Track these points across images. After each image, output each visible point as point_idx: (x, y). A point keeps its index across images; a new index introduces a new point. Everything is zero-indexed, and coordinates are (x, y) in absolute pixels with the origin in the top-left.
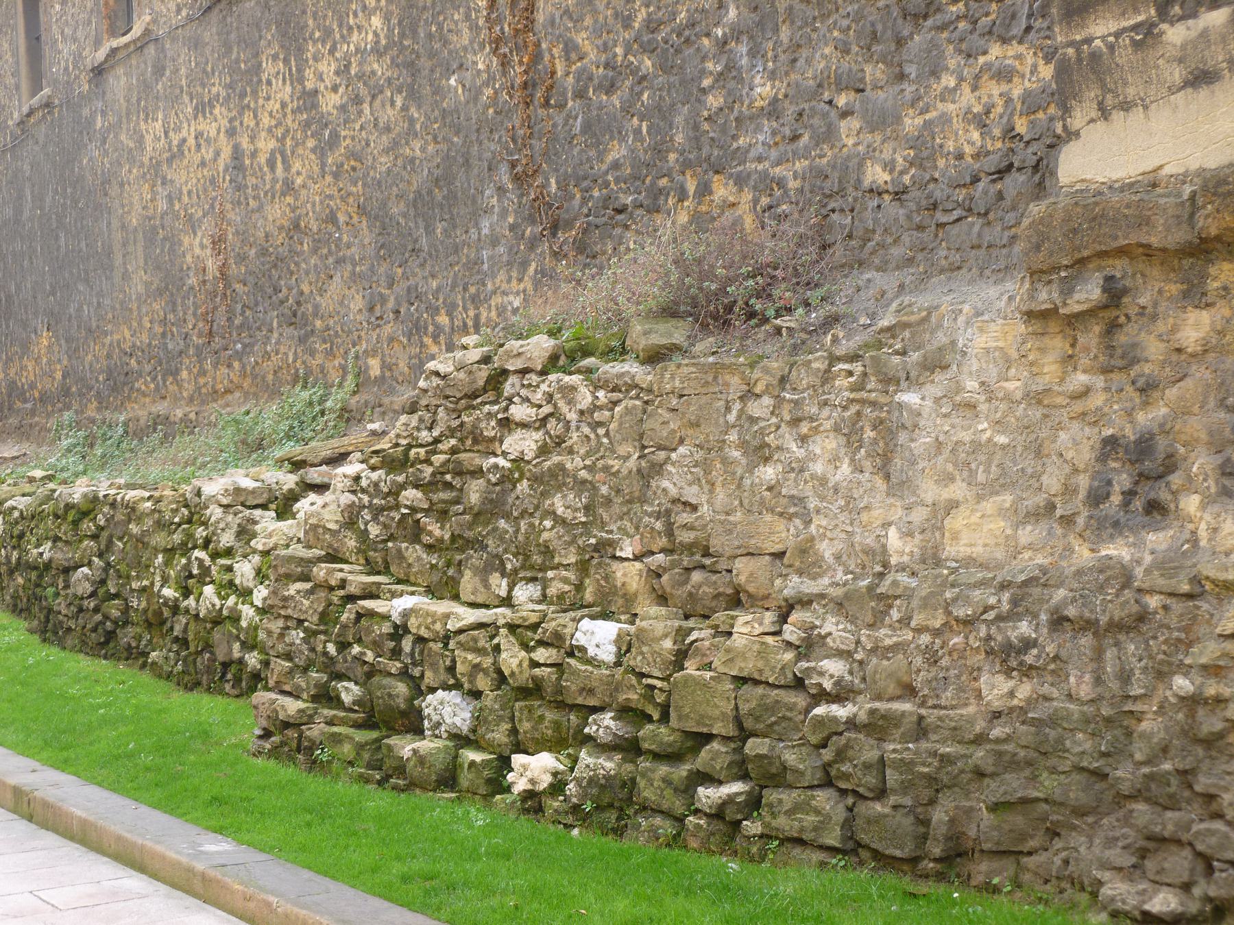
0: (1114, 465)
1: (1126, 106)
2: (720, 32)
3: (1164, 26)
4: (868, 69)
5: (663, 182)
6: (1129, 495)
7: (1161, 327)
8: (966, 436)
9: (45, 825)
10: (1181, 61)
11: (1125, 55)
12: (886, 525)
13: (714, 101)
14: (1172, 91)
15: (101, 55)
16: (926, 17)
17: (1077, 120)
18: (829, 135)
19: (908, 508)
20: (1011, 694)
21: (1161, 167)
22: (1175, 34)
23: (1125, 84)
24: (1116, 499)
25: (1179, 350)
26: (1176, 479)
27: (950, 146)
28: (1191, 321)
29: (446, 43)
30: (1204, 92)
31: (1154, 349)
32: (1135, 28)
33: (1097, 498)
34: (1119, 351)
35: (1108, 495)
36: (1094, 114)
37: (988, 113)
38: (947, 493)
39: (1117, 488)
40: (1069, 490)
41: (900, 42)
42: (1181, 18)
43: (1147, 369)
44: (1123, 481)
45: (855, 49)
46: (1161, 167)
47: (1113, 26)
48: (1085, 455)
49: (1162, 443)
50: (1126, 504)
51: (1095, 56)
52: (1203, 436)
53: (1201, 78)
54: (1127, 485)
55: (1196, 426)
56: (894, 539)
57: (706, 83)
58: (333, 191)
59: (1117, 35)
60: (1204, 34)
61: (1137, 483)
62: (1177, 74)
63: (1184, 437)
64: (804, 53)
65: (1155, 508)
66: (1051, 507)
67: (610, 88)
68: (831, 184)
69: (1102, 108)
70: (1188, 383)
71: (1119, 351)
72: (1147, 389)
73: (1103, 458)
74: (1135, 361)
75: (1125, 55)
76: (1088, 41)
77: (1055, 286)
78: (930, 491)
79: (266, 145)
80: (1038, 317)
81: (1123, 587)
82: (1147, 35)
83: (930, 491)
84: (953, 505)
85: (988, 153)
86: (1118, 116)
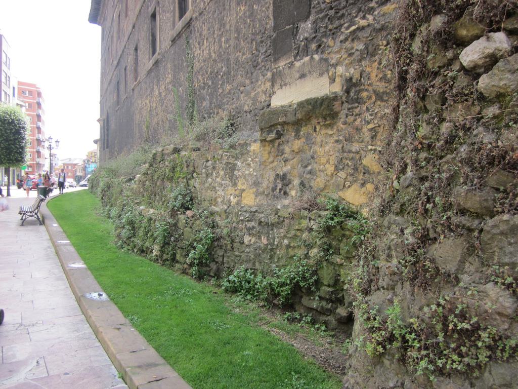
0: (278, 181)
1: (286, 85)
2: (222, 74)
3: (295, 62)
4: (246, 81)
5: (211, 111)
6: (281, 189)
7: (290, 144)
8: (247, 172)
9: (57, 255)
10: (298, 72)
11: (286, 71)
12: (231, 194)
13: (220, 91)
14: (296, 80)
15: (133, 87)
16: (257, 67)
17: (275, 89)
18: (238, 98)
19: (236, 190)
20: (250, 240)
21: (293, 101)
22: (298, 64)
23: (286, 78)
24: (278, 190)
25: (293, 151)
26: (290, 186)
27: (259, 99)
28: (296, 143)
29: (180, 79)
30: (303, 80)
31: (287, 149)
32: (289, 63)
33: (274, 189)
34: (280, 151)
35: (276, 189)
36: (279, 87)
37: (267, 90)
38: (243, 187)
39: (278, 188)
40: (268, 187)
41: (252, 74)
42: (300, 60)
43: (286, 155)
44: (279, 186)
45: (244, 76)
46: (293, 101)
47: (284, 63)
48: (272, 179)
49: (288, 176)
50: (280, 192)
51: (280, 71)
52: (297, 175)
53: (303, 76)
54: (280, 187)
55: (295, 172)
56: (232, 198)
57: (219, 86)
58: (163, 115)
59: (285, 65)
60: (304, 63)
61: (282, 186)
62: (297, 75)
63: (293, 175)
64: (235, 78)
65: (285, 193)
66: (264, 192)
67: (204, 89)
68: (238, 110)
69: (281, 86)
70: (295, 160)
71: (280, 151)
72: (286, 161)
73: (275, 179)
74: (283, 154)
75: (286, 71)
76: (279, 67)
77: (266, 133)
78: (240, 187)
79: (155, 105)
80: (263, 141)
81: (275, 214)
82: (292, 64)
83: (240, 187)
84: (244, 190)
85: (266, 101)
86: (284, 87)
